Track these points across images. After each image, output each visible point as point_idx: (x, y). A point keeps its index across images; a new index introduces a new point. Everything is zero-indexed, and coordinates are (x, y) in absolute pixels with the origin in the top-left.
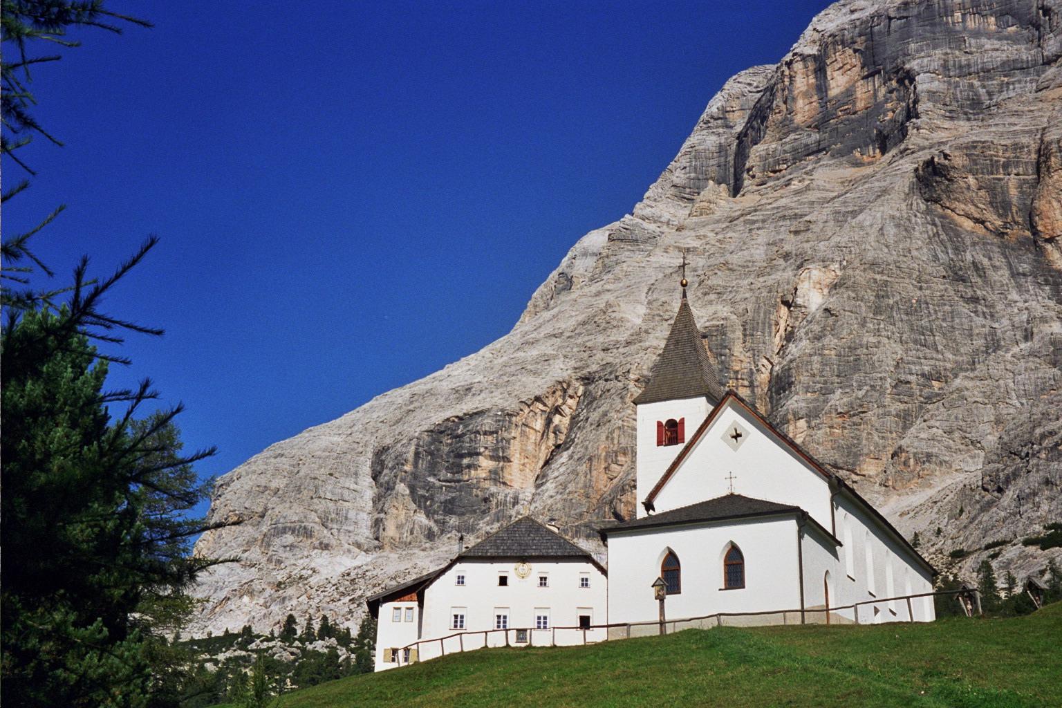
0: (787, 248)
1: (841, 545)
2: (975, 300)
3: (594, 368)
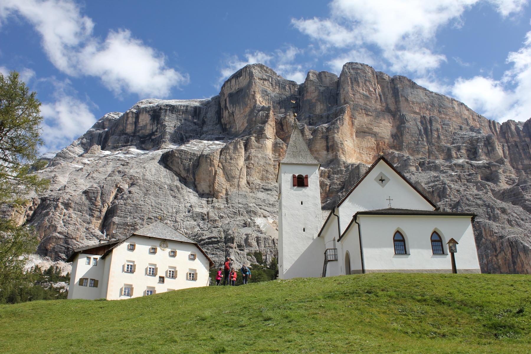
0: (120, 169)
1: (458, 243)
2: (175, 197)
3: (47, 196)
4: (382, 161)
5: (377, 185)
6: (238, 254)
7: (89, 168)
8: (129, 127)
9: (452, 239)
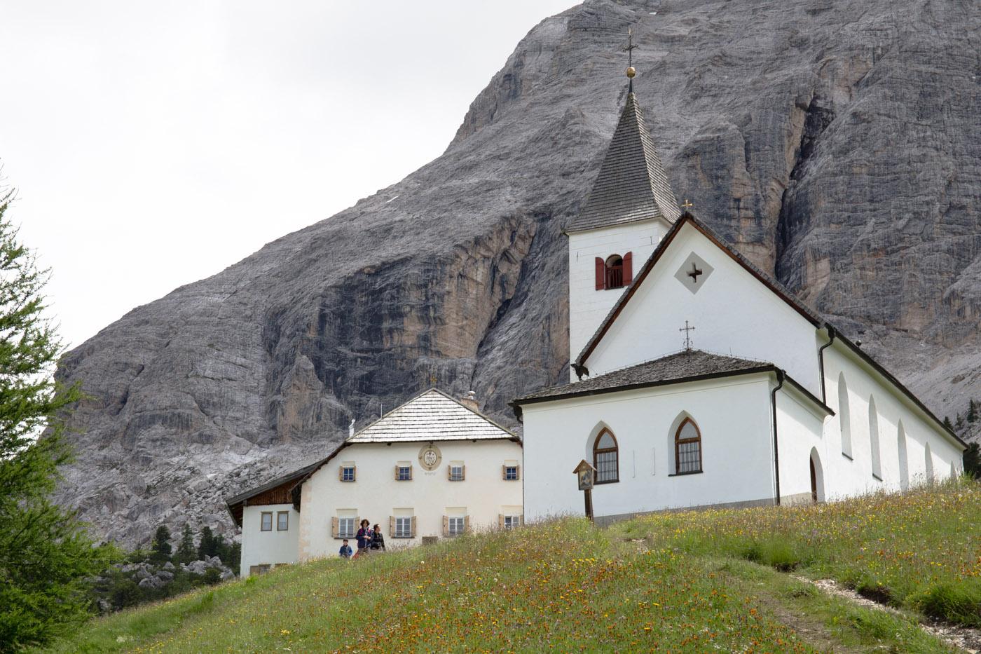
4: (687, 225)
7: (689, 54)
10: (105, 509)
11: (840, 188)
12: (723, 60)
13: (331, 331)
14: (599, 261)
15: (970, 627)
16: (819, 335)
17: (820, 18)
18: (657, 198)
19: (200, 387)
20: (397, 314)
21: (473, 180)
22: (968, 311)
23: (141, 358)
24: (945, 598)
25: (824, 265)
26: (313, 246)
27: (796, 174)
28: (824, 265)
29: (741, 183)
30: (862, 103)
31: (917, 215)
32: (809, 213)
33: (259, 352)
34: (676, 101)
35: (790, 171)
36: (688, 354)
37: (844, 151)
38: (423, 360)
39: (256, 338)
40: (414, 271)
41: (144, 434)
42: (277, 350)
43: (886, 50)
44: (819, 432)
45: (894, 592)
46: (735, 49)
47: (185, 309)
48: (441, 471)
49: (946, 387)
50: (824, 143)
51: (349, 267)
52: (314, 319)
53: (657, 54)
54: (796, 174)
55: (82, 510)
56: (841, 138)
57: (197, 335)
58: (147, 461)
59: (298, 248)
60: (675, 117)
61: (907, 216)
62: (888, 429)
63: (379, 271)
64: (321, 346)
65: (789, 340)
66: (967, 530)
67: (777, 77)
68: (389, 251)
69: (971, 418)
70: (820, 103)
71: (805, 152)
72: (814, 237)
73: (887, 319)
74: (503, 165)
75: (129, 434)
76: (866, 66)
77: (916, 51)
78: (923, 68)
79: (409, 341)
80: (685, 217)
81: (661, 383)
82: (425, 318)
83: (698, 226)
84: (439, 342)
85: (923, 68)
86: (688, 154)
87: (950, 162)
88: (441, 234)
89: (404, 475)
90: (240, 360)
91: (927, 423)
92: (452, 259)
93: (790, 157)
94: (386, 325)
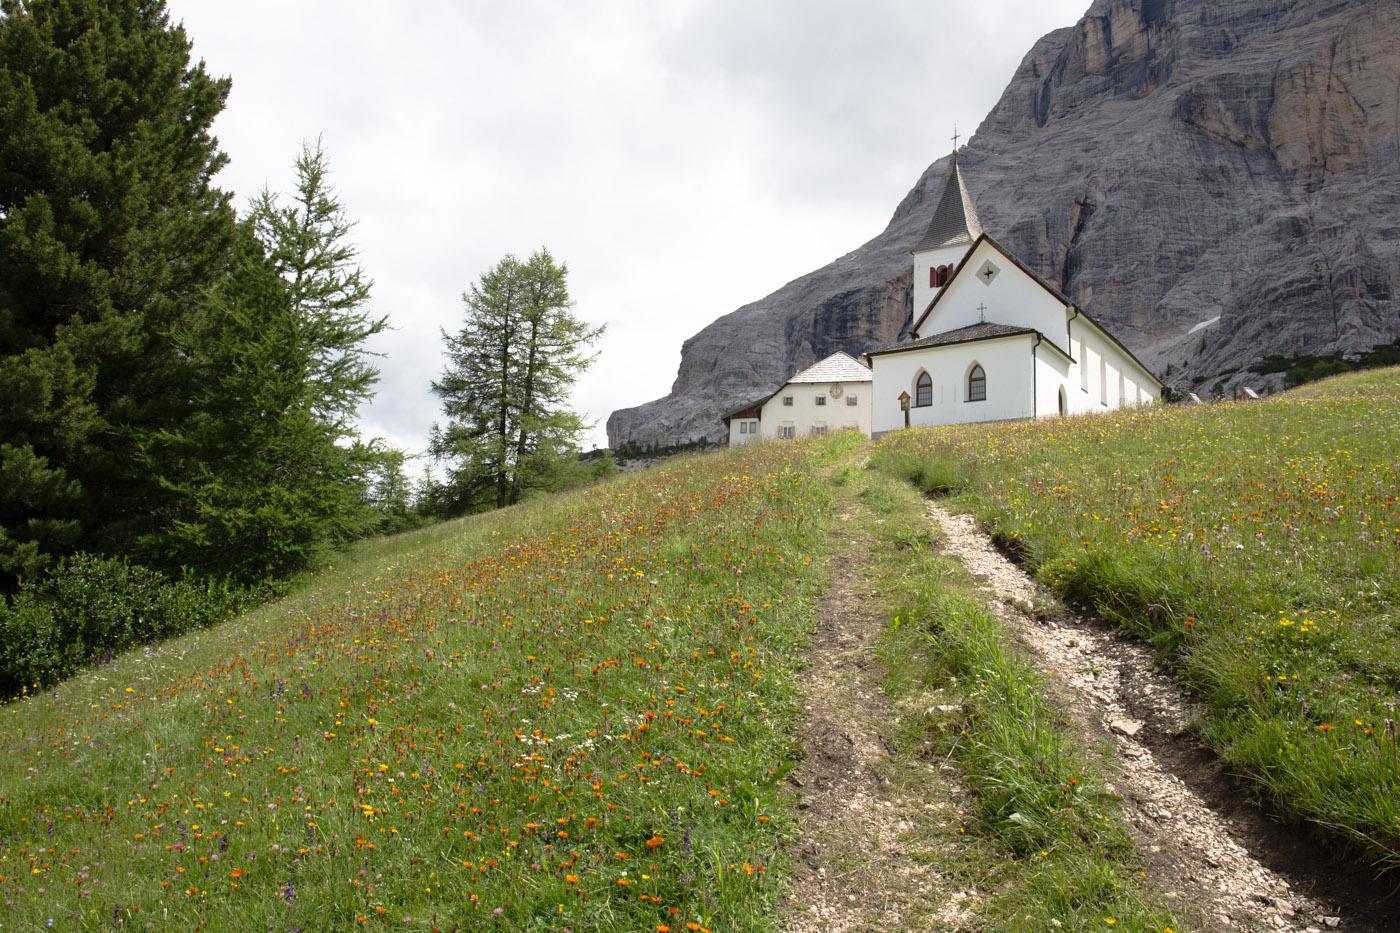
4: (984, 242)
5: (979, 284)
6: (1373, 310)
7: (1016, 176)
8: (1091, 55)
9: (855, 404)
10: (706, 420)
11: (1099, 248)
12: (1035, 178)
13: (820, 328)
14: (932, 269)
15: (1133, 639)
16: (1068, 312)
17: (1090, 154)
18: (970, 230)
19: (753, 357)
20: (855, 319)
21: (897, 247)
22: (1169, 315)
23: (724, 342)
24: (1099, 578)
25: (1089, 290)
26: (812, 283)
27: (1075, 240)
28: (1089, 290)
29: (1044, 246)
30: (1113, 200)
31: (1142, 262)
32: (1081, 262)
33: (783, 339)
34: (1008, 202)
35: (1071, 238)
36: (983, 324)
37: (1102, 227)
38: (869, 343)
39: (782, 332)
40: (864, 296)
41: (725, 382)
42: (792, 338)
43: (1126, 171)
44: (1066, 374)
45: (1035, 547)
46: (1041, 172)
47: (745, 317)
48: (843, 399)
49: (1154, 357)
50: (1090, 223)
51: (830, 294)
52: (812, 322)
53: (998, 176)
54: (1075, 240)
55: (694, 420)
56: (1100, 220)
57: (751, 331)
58: (727, 395)
59: (804, 285)
60: (1007, 211)
61: (1137, 263)
62: (1113, 373)
63: (846, 296)
64: (815, 336)
65: (1050, 315)
66: (1150, 452)
67: (1066, 187)
68: (851, 285)
69: (1168, 374)
70: (1089, 201)
71: (1080, 228)
72: (1084, 275)
73: (1124, 320)
74: (913, 238)
75: (717, 382)
76: (1115, 180)
77: (1143, 171)
78: (1147, 181)
79: (861, 333)
80: (983, 237)
81: (961, 342)
82: (870, 321)
83: (991, 242)
84: (877, 334)
85: (1147, 181)
86: (1014, 230)
87: (1161, 233)
88: (879, 276)
89: (821, 401)
90: (773, 344)
91: (1142, 374)
92: (884, 290)
93: (1071, 232)
94: (849, 324)
